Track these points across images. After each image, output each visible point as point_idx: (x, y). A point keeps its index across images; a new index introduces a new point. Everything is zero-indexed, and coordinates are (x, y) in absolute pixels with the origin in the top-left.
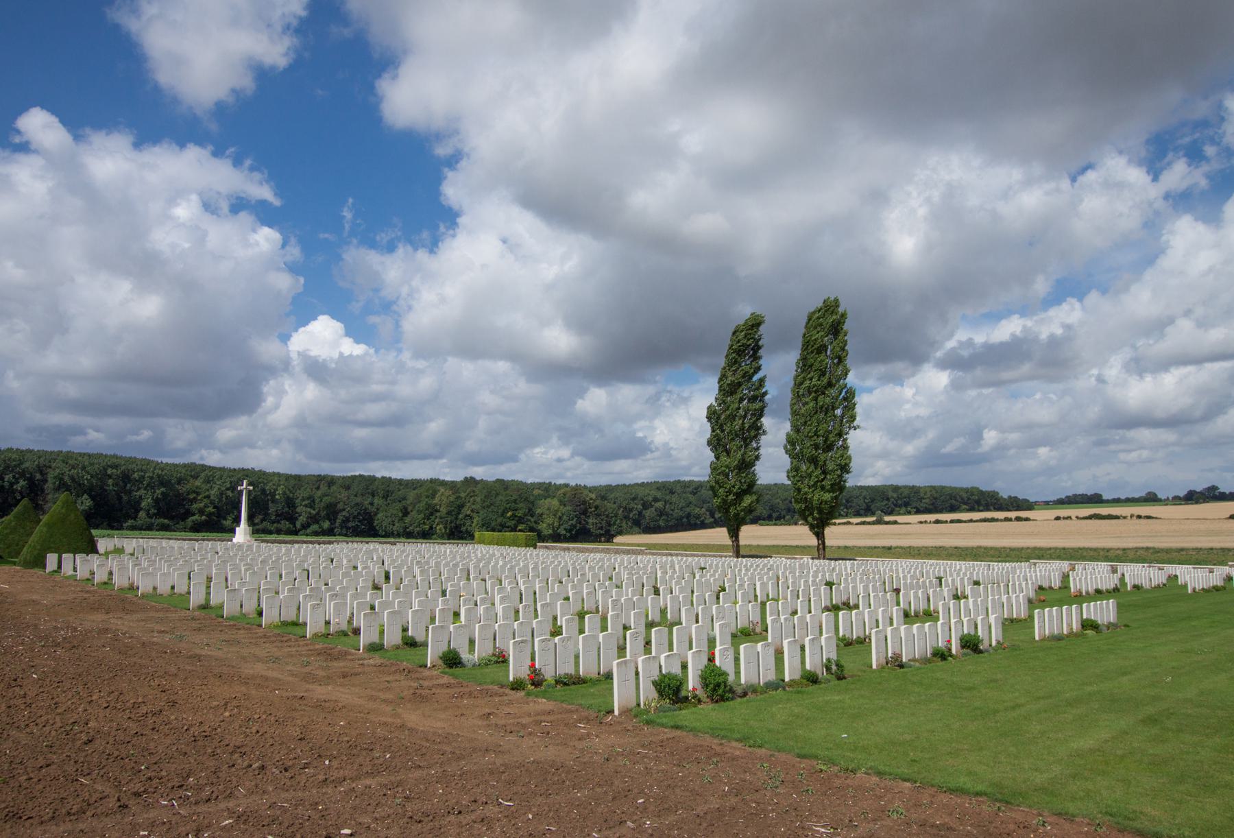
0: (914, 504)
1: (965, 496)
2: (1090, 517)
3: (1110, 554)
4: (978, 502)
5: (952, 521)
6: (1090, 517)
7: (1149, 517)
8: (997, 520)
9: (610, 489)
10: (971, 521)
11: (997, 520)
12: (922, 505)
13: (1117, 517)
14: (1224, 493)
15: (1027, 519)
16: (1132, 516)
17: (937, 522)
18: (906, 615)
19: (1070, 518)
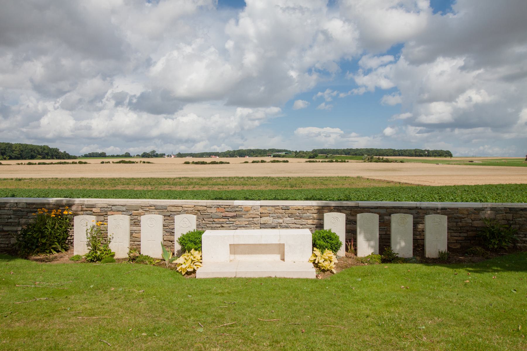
0: (8, 154)
1: (40, 150)
2: (120, 162)
3: (171, 182)
4: (47, 154)
5: (39, 164)
6: (120, 162)
7: (149, 163)
8: (68, 163)
9: (407, 150)
10: (52, 163)
11: (68, 163)
12: (13, 155)
13: (133, 163)
14: (157, 154)
15: (85, 163)
16: (140, 162)
17: (60, 163)
18: (331, 262)
19: (109, 162)
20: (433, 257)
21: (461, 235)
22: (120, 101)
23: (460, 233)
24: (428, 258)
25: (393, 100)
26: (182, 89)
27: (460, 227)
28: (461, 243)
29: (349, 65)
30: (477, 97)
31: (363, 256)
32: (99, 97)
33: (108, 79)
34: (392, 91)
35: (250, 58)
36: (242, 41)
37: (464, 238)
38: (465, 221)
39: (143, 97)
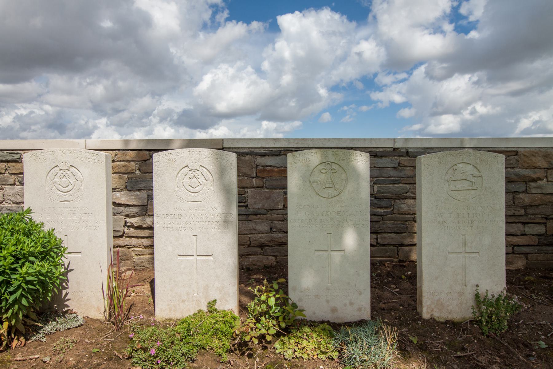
20: (450, 317)
21: (528, 229)
22: (164, 118)
23: (524, 224)
24: (432, 323)
25: (406, 113)
26: (222, 107)
27: (525, 207)
28: (526, 254)
29: (369, 82)
30: (481, 109)
31: (177, 315)
32: (148, 114)
33: (157, 97)
34: (406, 105)
35: (287, 79)
36: (278, 64)
37: (536, 239)
38: (540, 187)
39: (185, 113)
